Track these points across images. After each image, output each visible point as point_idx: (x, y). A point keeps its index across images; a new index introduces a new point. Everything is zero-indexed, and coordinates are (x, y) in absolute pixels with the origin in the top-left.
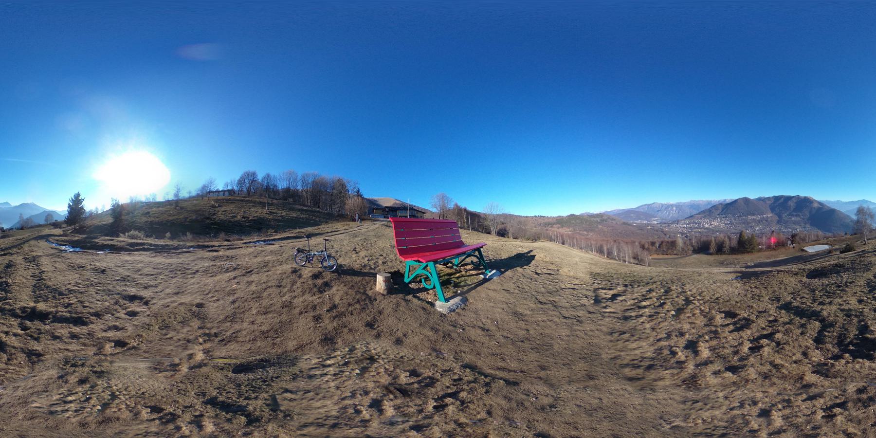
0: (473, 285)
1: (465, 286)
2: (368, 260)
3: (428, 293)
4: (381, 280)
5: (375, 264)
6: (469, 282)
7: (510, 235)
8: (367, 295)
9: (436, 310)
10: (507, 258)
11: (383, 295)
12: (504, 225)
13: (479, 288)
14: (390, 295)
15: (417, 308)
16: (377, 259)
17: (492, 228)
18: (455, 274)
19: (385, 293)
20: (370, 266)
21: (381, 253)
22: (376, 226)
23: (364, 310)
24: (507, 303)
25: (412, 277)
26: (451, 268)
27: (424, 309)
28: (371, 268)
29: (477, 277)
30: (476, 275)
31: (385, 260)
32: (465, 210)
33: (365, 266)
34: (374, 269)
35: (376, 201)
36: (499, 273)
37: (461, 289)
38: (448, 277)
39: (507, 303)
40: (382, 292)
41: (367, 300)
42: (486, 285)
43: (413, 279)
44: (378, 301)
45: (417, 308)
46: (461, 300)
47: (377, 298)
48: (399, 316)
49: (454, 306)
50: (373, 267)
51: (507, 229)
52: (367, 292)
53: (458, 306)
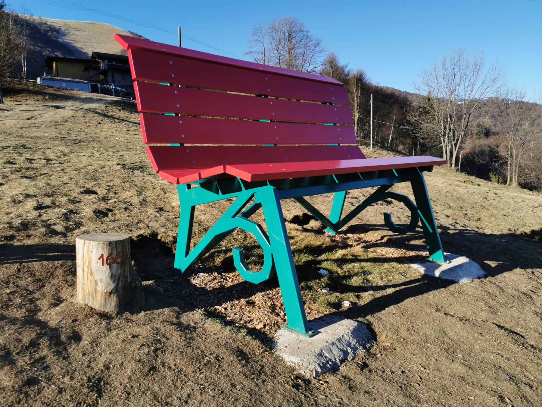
0: (390, 291)
1: (364, 289)
2: (39, 207)
3: (251, 303)
4: (95, 256)
5: (66, 217)
6: (375, 279)
7: (512, 173)
8: (43, 325)
9: (278, 360)
10: (502, 236)
11: (104, 316)
12: (491, 141)
13: (409, 303)
14: (127, 314)
15: (222, 352)
16: (73, 201)
17: (446, 145)
18: (330, 249)
19: (111, 307)
20: (47, 225)
21: (90, 185)
22: (67, 112)
23: (32, 390)
24: (512, 378)
25: (195, 253)
26: (319, 232)
27: (242, 355)
28: (54, 233)
29: (403, 267)
30: (400, 260)
31: (103, 206)
32: (360, 80)
33: (25, 226)
34: (64, 235)
35: (57, 31)
36: (476, 268)
37: (351, 296)
38: (311, 258)
39: (512, 378)
40: (98, 304)
41: (44, 342)
42: (433, 296)
43: (200, 258)
44: (85, 341)
45: (222, 352)
46: (355, 333)
47: (83, 329)
48: (166, 391)
49: (336, 351)
50: (58, 228)
51: (502, 152)
52: (41, 316)
53: (346, 353)
